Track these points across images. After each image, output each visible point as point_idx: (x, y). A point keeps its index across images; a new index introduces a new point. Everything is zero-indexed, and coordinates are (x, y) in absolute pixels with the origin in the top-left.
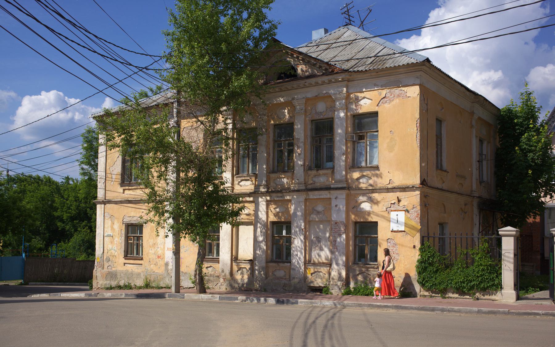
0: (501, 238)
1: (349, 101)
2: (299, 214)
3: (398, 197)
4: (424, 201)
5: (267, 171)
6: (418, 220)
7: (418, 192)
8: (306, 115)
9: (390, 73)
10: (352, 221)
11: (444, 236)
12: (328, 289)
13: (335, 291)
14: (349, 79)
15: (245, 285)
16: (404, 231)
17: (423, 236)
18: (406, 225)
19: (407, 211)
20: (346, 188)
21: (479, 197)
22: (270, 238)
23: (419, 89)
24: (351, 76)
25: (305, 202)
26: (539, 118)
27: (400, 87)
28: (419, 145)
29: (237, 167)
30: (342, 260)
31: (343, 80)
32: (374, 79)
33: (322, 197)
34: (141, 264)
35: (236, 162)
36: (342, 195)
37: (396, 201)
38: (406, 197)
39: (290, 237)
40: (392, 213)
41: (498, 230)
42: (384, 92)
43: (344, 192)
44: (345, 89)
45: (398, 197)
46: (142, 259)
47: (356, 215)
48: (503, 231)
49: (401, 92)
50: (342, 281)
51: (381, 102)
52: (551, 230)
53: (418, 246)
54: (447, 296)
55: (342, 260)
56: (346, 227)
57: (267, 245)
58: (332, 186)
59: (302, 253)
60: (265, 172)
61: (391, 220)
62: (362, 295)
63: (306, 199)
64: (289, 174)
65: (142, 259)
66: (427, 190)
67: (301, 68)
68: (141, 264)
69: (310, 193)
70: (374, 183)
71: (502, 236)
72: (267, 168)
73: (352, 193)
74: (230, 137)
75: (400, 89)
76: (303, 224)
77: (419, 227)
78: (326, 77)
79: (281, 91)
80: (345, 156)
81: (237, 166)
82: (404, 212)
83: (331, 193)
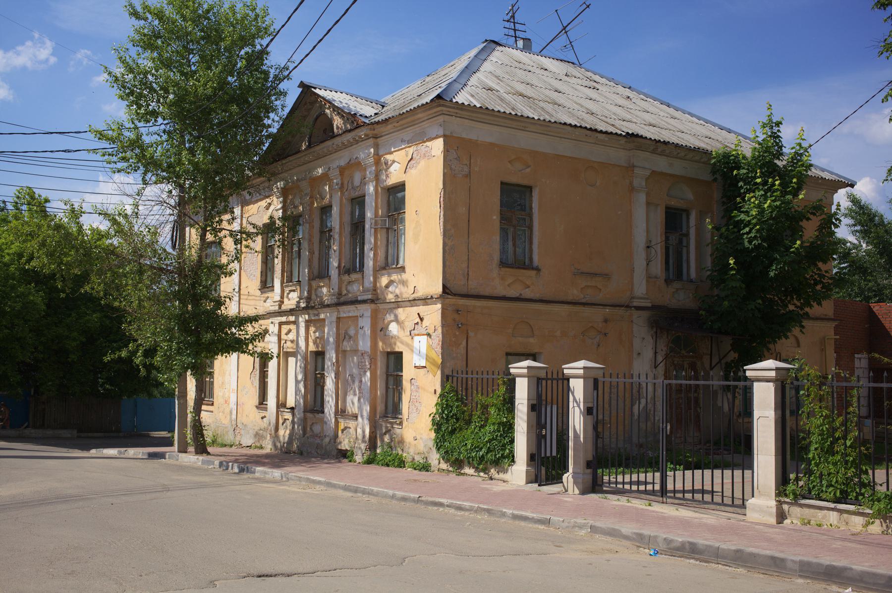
0: (753, 385)
1: (381, 166)
2: (331, 340)
3: (418, 314)
4: (454, 320)
5: (309, 277)
6: (439, 350)
7: (439, 306)
8: (342, 193)
9: (413, 121)
10: (381, 352)
11: (667, 382)
12: (353, 454)
13: (358, 458)
14: (377, 135)
15: (285, 445)
16: (425, 367)
17: (447, 375)
18: (428, 358)
19: (429, 335)
20: (368, 301)
21: (654, 308)
22: (311, 377)
23: (443, 143)
24: (374, 130)
25: (337, 322)
26: (785, 147)
27: (424, 142)
28: (442, 230)
29: (289, 273)
30: (366, 410)
31: (367, 137)
32: (400, 132)
33: (351, 315)
34: (212, 412)
35: (287, 265)
36: (366, 310)
37: (418, 320)
38: (429, 313)
39: (324, 374)
40: (417, 338)
41: (510, 366)
42: (411, 150)
43: (369, 307)
44: (372, 150)
45: (418, 314)
46: (212, 404)
47: (384, 343)
48: (752, 370)
49: (426, 149)
50: (366, 443)
51: (408, 167)
52: (563, 366)
53: (439, 391)
54: (462, 472)
55: (366, 410)
56: (373, 360)
57: (305, 387)
58: (359, 298)
59: (333, 399)
60: (307, 278)
61: (414, 350)
62: (382, 465)
63: (338, 319)
64: (326, 280)
65: (212, 404)
66: (452, 300)
67: (338, 122)
68: (212, 412)
69: (345, 308)
70: (400, 294)
71: (753, 381)
72: (309, 272)
73: (380, 308)
74: (780, 163)
75: (425, 144)
76: (334, 356)
77: (440, 361)
78: (350, 134)
79: (319, 158)
80: (372, 252)
81: (289, 269)
82: (426, 336)
83: (358, 308)
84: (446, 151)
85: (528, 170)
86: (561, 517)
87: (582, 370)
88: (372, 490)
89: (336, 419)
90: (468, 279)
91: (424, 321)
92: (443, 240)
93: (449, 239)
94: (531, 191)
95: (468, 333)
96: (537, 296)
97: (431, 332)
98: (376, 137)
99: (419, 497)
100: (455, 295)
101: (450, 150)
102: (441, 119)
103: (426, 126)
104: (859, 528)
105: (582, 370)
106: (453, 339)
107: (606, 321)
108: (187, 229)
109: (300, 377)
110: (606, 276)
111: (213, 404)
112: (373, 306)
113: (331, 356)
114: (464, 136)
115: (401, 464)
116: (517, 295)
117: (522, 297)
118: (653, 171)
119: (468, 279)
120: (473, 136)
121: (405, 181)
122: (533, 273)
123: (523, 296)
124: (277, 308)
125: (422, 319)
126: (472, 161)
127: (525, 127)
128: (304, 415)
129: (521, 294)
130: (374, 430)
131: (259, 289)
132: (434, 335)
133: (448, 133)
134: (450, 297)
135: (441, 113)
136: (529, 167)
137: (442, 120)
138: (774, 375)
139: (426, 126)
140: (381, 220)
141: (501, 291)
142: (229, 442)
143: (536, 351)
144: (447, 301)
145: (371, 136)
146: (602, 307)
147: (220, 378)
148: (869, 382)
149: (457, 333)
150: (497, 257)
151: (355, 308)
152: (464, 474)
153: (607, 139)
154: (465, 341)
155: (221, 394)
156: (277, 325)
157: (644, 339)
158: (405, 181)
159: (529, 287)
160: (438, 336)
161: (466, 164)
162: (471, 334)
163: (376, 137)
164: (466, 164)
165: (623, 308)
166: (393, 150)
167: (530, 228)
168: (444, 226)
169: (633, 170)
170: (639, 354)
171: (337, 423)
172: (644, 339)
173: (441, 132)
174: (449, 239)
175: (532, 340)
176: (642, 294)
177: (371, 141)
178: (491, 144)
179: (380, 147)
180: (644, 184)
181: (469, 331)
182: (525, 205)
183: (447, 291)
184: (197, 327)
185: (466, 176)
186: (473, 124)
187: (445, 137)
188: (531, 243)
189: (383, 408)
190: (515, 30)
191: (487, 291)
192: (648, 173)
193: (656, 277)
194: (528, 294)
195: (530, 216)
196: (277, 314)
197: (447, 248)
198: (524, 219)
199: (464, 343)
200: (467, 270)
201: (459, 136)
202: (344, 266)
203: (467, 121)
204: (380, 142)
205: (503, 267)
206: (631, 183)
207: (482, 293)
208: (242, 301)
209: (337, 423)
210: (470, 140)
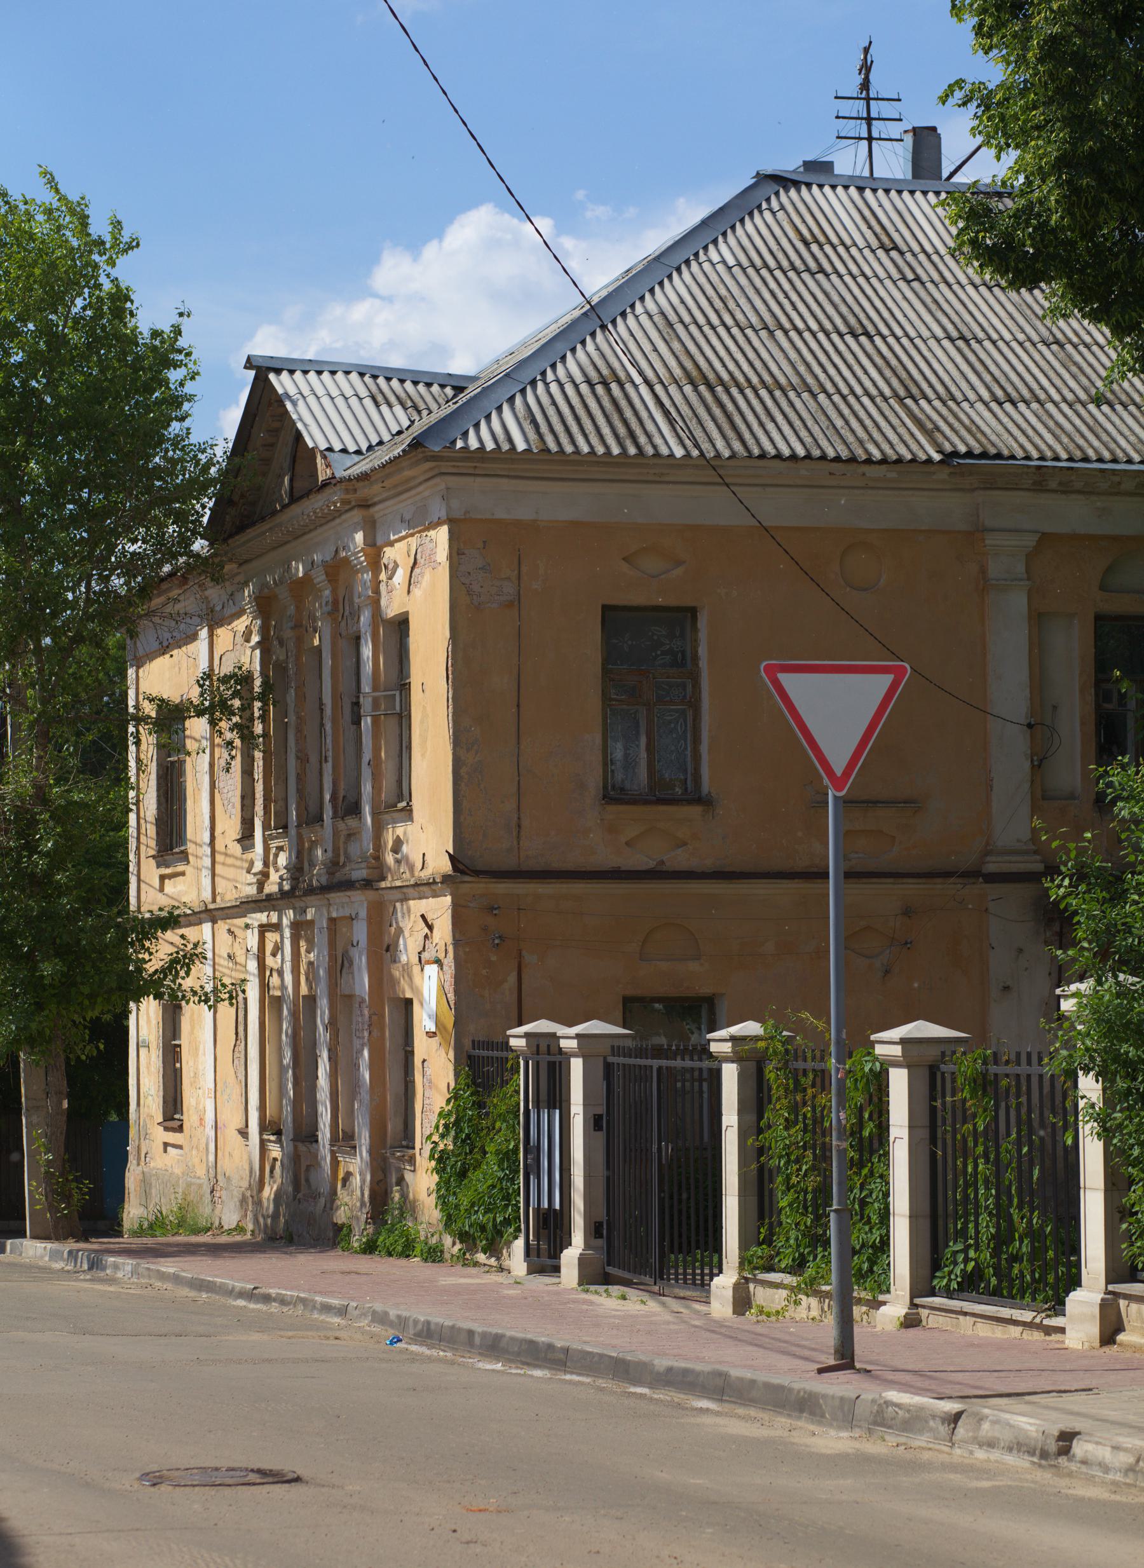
3: (423, 916)
4: (485, 929)
27: (428, 529)
29: (281, 803)
37: (426, 930)
42: (413, 541)
45: (423, 916)
53: (452, 1085)
78: (319, 496)
83: (353, 899)
84: (455, 554)
85: (679, 571)
86: (248, 1282)
87: (575, 1041)
88: (214, 1283)
89: (333, 1153)
90: (518, 837)
91: (435, 931)
92: (454, 754)
93: (468, 750)
94: (694, 618)
95: (520, 955)
96: (708, 863)
97: (441, 955)
98: (365, 505)
99: (255, 1288)
100: (477, 873)
101: (466, 552)
102: (441, 483)
103: (426, 494)
104: (1018, 1335)
105: (575, 1041)
106: (484, 972)
107: (907, 912)
108: (131, 672)
109: (287, 1059)
110: (911, 804)
111: (181, 1126)
112: (370, 894)
113: (323, 1004)
114: (501, 514)
115: (407, 1251)
116: (651, 864)
117: (664, 868)
118: (1043, 534)
119: (518, 837)
120: (524, 513)
121: (407, 613)
122: (695, 811)
123: (669, 866)
124: (252, 891)
125: (430, 927)
126: (524, 569)
127: (662, 474)
128: (295, 1147)
129: (662, 862)
130: (381, 1177)
131: (239, 841)
132: (445, 962)
133: (458, 514)
134: (467, 878)
135: (436, 471)
136: (679, 563)
137: (443, 486)
138: (730, 1050)
139: (426, 494)
140: (385, 696)
141: (605, 857)
142: (203, 1223)
143: (706, 990)
144: (465, 888)
145: (353, 503)
146: (891, 880)
147: (191, 1063)
148: (560, 1063)
149: (494, 958)
150: (594, 781)
151: (347, 900)
152: (476, 1264)
153: (894, 475)
154: (514, 974)
155: (193, 1102)
156: (256, 931)
157: (1020, 950)
158: (407, 613)
159: (685, 844)
160: (449, 962)
161: (508, 579)
162: (529, 958)
163: (365, 505)
164: (508, 579)
165: (952, 880)
166: (392, 538)
167: (695, 705)
168: (456, 722)
169: (984, 540)
170: (1006, 988)
171: (335, 1163)
172: (1020, 951)
173: (443, 514)
174: (468, 750)
175: (693, 966)
176: (1019, 841)
177: (356, 515)
178: (575, 524)
179: (378, 525)
180: (1021, 568)
181: (524, 953)
182: (683, 653)
183: (461, 867)
184: (31, 951)
185: (510, 605)
186: (521, 485)
187: (452, 522)
188: (697, 740)
189: (401, 1127)
190: (869, 120)
191: (573, 860)
192: (1030, 541)
193: (1072, 796)
194: (681, 859)
195: (695, 678)
196: (253, 905)
197: (463, 771)
198: (684, 686)
199: (512, 979)
200: (516, 816)
201: (488, 516)
202: (344, 797)
203: (505, 481)
204: (377, 516)
205: (608, 803)
206: (983, 571)
207: (556, 865)
208: (219, 869)
209: (335, 1163)
210: (517, 523)
